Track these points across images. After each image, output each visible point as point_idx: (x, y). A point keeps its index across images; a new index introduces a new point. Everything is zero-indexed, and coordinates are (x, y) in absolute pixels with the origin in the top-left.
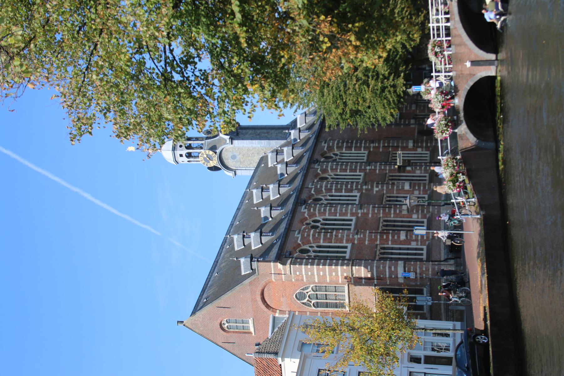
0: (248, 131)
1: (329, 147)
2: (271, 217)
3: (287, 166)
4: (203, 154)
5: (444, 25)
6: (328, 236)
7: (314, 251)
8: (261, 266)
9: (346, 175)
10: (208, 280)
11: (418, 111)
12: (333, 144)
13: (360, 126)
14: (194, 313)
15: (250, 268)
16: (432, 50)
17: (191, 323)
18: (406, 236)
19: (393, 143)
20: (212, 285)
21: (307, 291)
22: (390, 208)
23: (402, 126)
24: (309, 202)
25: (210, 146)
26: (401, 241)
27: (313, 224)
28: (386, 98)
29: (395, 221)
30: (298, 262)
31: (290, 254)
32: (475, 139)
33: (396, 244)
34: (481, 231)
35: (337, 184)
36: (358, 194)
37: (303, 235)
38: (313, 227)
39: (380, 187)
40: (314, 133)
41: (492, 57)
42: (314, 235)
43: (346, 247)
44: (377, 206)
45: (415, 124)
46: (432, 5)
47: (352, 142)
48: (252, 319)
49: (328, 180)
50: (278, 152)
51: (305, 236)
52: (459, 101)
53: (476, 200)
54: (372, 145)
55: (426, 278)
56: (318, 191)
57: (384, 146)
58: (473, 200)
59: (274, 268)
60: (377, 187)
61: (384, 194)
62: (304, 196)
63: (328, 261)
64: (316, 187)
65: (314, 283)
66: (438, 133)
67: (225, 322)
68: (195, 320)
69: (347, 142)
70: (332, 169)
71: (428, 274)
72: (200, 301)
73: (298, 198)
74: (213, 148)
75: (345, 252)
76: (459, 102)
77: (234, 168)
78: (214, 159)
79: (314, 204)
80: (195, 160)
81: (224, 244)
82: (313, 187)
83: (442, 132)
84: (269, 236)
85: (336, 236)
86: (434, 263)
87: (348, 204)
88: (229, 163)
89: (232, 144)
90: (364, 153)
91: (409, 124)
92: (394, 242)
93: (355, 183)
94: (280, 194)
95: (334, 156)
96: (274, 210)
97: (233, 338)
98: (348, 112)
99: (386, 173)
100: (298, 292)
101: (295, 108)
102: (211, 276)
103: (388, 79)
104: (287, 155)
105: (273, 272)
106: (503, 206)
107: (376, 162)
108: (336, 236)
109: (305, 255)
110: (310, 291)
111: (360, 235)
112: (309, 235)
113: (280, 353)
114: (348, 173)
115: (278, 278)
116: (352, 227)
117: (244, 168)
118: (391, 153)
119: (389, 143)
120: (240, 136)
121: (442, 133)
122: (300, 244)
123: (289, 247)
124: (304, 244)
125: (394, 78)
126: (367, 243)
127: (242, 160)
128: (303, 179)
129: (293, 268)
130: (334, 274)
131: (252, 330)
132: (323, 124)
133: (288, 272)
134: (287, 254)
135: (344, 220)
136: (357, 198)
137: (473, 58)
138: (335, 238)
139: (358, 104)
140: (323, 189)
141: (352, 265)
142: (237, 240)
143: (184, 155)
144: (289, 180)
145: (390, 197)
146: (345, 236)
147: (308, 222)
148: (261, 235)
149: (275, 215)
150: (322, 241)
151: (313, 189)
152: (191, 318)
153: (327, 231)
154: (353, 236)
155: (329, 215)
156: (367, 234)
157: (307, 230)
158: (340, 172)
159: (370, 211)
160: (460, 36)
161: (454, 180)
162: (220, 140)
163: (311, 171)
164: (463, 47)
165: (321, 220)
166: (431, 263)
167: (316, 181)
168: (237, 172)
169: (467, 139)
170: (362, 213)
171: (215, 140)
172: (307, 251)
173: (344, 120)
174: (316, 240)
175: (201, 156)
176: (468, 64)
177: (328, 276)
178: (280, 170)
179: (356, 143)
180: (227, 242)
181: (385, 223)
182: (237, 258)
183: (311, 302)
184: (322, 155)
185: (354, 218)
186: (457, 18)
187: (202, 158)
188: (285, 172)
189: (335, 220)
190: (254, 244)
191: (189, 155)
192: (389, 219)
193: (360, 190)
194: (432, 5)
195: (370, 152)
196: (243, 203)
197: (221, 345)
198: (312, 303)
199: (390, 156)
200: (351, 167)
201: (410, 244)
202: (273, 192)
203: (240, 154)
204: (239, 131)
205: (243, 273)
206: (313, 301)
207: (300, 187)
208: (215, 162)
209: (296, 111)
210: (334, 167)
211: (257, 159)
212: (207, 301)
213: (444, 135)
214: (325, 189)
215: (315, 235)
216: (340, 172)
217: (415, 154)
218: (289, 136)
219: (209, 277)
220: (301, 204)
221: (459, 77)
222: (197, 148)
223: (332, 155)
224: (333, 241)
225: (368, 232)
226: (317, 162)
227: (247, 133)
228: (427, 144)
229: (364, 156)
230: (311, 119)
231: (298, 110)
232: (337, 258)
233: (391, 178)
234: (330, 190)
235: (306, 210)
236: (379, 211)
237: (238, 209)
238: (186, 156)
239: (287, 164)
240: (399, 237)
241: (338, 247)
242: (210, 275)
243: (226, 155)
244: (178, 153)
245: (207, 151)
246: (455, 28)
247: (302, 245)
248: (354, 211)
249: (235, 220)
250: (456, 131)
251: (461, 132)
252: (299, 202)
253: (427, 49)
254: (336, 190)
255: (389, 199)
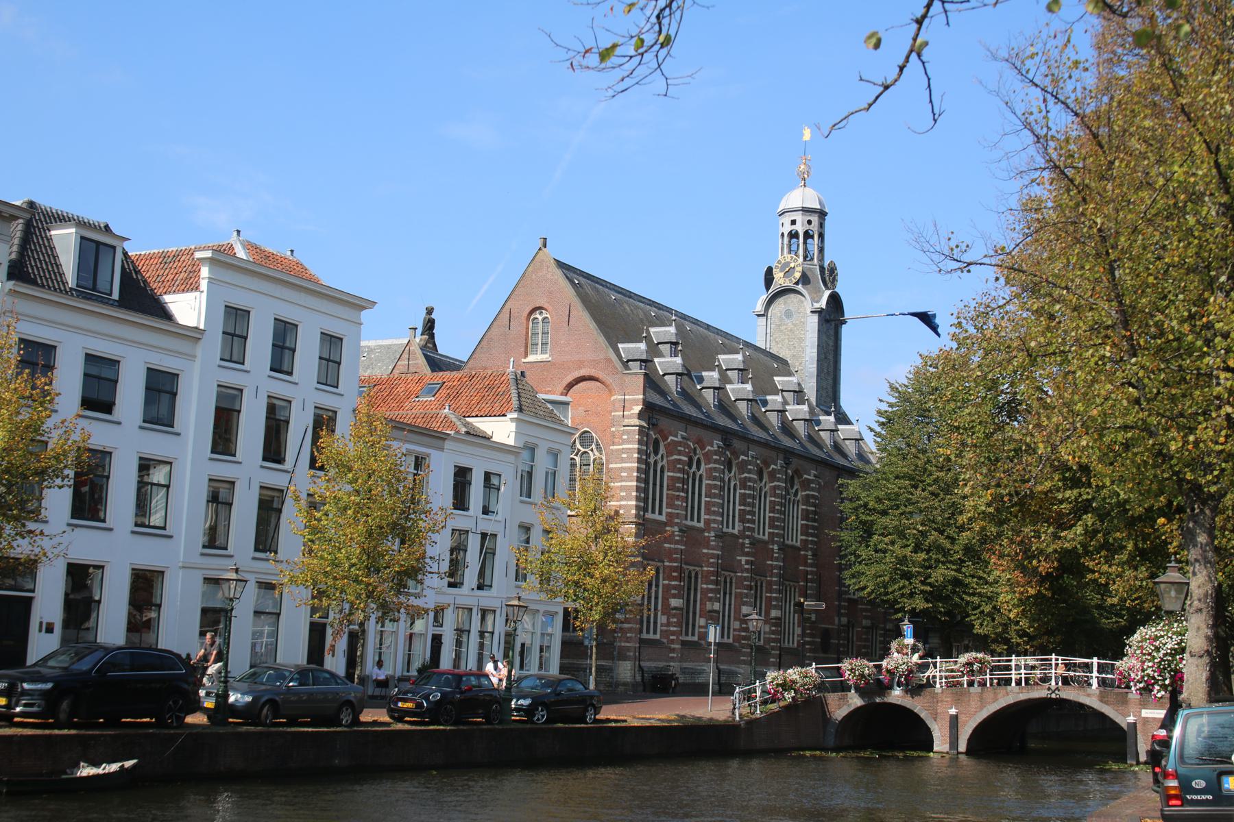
0: (832, 338)
1: (810, 481)
2: (703, 388)
3: (778, 411)
4: (796, 261)
5: (1014, 677)
6: (677, 485)
7: (656, 462)
8: (637, 381)
9: (734, 503)
10: (604, 284)
11: (860, 629)
12: (813, 489)
13: (845, 535)
14: (561, 265)
15: (630, 358)
16: (976, 658)
17: (543, 261)
18: (675, 608)
19: (811, 588)
20: (597, 290)
21: (595, 450)
22: (717, 583)
23: (837, 603)
24: (728, 453)
25: (809, 274)
26: (668, 600)
27: (696, 458)
28: (893, 581)
29: (696, 590)
30: (642, 438)
31: (653, 425)
32: (840, 719)
33: (663, 591)
34: (717, 720)
35: (753, 497)
36: (736, 531)
37: (679, 444)
38: (691, 459)
39: (746, 567)
40: (829, 456)
41: (962, 747)
42: (679, 461)
43: (660, 513)
44: (720, 561)
45: (840, 625)
46: (1042, 660)
47: (814, 520)
48: (550, 359)
49: (759, 482)
50: (799, 395)
51: (679, 448)
52: (898, 696)
53: (758, 716)
54: (810, 553)
55: (615, 638)
56: (743, 467)
57: (807, 573)
58: (758, 712)
59: (634, 399)
60: (747, 562)
61: (736, 572)
62: (737, 444)
63: (643, 485)
64: (749, 463)
65: (608, 462)
66: (851, 664)
67: (544, 315)
68: (548, 267)
69: (815, 513)
70: (775, 488)
71: (620, 641)
72: (574, 272)
73: (733, 433)
74: (805, 279)
75: (653, 512)
76: (896, 695)
77: (769, 315)
78: (787, 280)
79: (724, 461)
80: (785, 246)
81: (655, 307)
82: (750, 459)
83: (852, 669)
84: (677, 388)
85: (678, 497)
86: (637, 650)
87: (722, 515)
88: (779, 306)
89: (812, 312)
90: (796, 539)
91: (840, 615)
92: (667, 588)
93: (782, 532)
94: (735, 401)
95: (794, 490)
96: (714, 393)
97: (518, 327)
98: (869, 518)
99: (766, 577)
100: (594, 435)
101: (878, 429)
102: (610, 289)
103: (923, 583)
104: (797, 411)
105: (626, 397)
106: (748, 754)
107: (784, 560)
108: (678, 497)
109: (651, 449)
110: (594, 455)
111: (679, 536)
112: (680, 453)
113: (523, 417)
114: (768, 514)
115: (617, 405)
116: (689, 523)
117: (768, 331)
118: (796, 584)
119: (812, 581)
120: (824, 325)
121: (851, 670)
122: (667, 439)
123: (664, 422)
124: (667, 446)
125: (926, 592)
126: (666, 545)
127: (783, 328)
128: (762, 441)
129: (634, 430)
130: (623, 494)
131: (531, 358)
132: (852, 473)
133: (626, 422)
134: (655, 420)
135: (699, 509)
136: (730, 530)
137: (962, 719)
138: (674, 495)
139: (882, 534)
140: (746, 475)
141: (637, 524)
142: (667, 332)
143: (794, 227)
144: (757, 415)
145: (731, 583)
146: (677, 511)
147: (698, 451)
148: (678, 374)
149: (705, 395)
150: (671, 474)
151: (746, 458)
152: (552, 261)
153: (686, 482)
154: (677, 524)
155: (707, 485)
156: (679, 547)
157: (687, 450)
158: (770, 501)
159: (712, 551)
160: (995, 700)
161: (786, 686)
162: (819, 291)
163: (773, 454)
164: (979, 704)
165: (701, 472)
166: (638, 645)
167: (758, 462)
168: (764, 319)
169: (840, 707)
170: (709, 537)
171: (818, 282)
172: (656, 452)
173: (856, 509)
174: (673, 466)
175: (792, 257)
176: (953, 711)
177: (619, 484)
178: (773, 400)
179: (813, 528)
180: (662, 314)
181: (693, 575)
182: (646, 337)
183: (576, 455)
184: (797, 473)
185: (702, 525)
186: (1023, 696)
187: (788, 260)
188: (769, 408)
189: (700, 495)
190: (663, 362)
191: (793, 235)
192: (699, 580)
193: (742, 535)
194: (1042, 660)
195: (799, 549)
196: (718, 334)
197: (506, 307)
198: (575, 457)
199: (792, 584)
200: (778, 519)
201: (663, 614)
202: (740, 389)
203: (793, 324)
204: (833, 323)
205: (620, 346)
206: (577, 459)
207: (750, 436)
208: (780, 280)
209: (872, 430)
210: (778, 492)
211: (783, 353)
212: (575, 284)
213: (848, 672)
214: (746, 477)
215: (679, 464)
216: (770, 501)
217: (794, 623)
218: (822, 410)
219: (608, 285)
220: (725, 439)
221: (933, 697)
222: (806, 250)
223: (795, 488)
224: (670, 492)
225: (683, 547)
226: (786, 464)
227: (828, 337)
228: (809, 643)
229: (792, 540)
230: (850, 448)
231: (873, 433)
232: (646, 500)
233: (759, 584)
234: (744, 486)
235: (715, 448)
236: (712, 565)
237: (708, 327)
238: (791, 231)
239: (783, 412)
240: (674, 596)
241: (661, 501)
242: (612, 287)
243: (792, 301)
244: (799, 217)
245: (800, 269)
246: (1008, 694)
247: (666, 443)
248: (712, 525)
249: (692, 322)
250: (853, 691)
251: (851, 698)
252: (727, 435)
253: (977, 651)
254: (743, 496)
255: (728, 580)
